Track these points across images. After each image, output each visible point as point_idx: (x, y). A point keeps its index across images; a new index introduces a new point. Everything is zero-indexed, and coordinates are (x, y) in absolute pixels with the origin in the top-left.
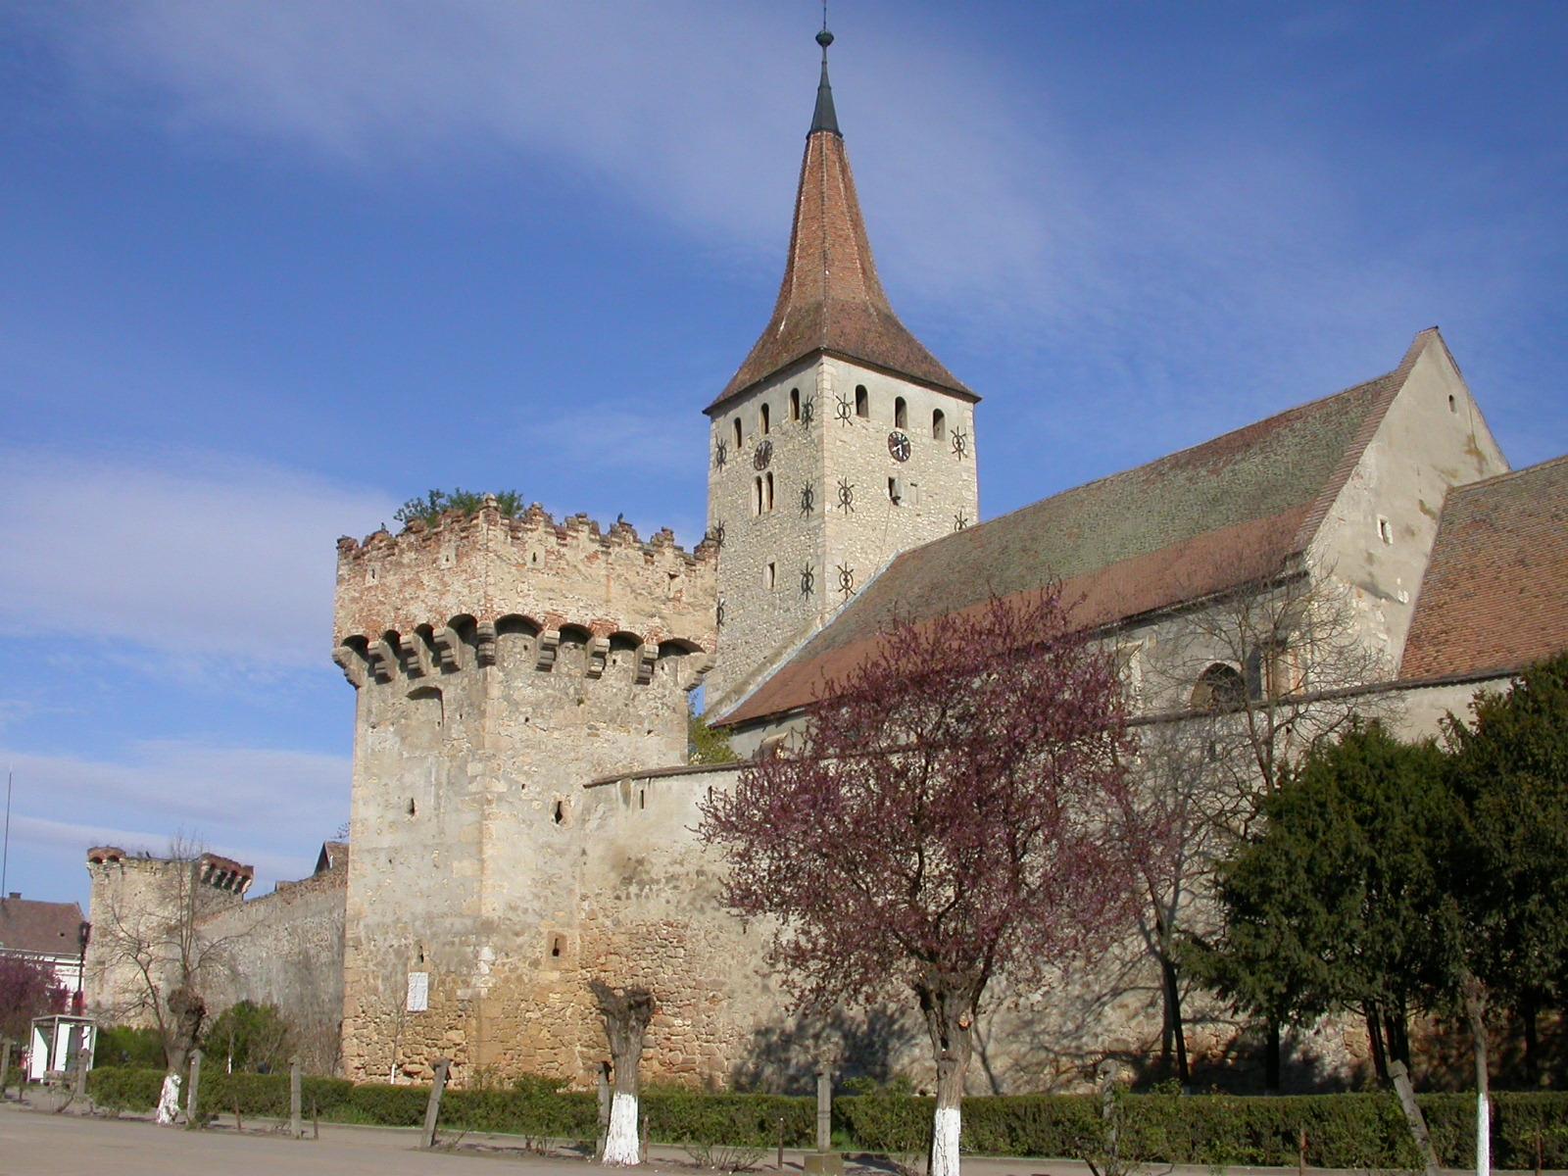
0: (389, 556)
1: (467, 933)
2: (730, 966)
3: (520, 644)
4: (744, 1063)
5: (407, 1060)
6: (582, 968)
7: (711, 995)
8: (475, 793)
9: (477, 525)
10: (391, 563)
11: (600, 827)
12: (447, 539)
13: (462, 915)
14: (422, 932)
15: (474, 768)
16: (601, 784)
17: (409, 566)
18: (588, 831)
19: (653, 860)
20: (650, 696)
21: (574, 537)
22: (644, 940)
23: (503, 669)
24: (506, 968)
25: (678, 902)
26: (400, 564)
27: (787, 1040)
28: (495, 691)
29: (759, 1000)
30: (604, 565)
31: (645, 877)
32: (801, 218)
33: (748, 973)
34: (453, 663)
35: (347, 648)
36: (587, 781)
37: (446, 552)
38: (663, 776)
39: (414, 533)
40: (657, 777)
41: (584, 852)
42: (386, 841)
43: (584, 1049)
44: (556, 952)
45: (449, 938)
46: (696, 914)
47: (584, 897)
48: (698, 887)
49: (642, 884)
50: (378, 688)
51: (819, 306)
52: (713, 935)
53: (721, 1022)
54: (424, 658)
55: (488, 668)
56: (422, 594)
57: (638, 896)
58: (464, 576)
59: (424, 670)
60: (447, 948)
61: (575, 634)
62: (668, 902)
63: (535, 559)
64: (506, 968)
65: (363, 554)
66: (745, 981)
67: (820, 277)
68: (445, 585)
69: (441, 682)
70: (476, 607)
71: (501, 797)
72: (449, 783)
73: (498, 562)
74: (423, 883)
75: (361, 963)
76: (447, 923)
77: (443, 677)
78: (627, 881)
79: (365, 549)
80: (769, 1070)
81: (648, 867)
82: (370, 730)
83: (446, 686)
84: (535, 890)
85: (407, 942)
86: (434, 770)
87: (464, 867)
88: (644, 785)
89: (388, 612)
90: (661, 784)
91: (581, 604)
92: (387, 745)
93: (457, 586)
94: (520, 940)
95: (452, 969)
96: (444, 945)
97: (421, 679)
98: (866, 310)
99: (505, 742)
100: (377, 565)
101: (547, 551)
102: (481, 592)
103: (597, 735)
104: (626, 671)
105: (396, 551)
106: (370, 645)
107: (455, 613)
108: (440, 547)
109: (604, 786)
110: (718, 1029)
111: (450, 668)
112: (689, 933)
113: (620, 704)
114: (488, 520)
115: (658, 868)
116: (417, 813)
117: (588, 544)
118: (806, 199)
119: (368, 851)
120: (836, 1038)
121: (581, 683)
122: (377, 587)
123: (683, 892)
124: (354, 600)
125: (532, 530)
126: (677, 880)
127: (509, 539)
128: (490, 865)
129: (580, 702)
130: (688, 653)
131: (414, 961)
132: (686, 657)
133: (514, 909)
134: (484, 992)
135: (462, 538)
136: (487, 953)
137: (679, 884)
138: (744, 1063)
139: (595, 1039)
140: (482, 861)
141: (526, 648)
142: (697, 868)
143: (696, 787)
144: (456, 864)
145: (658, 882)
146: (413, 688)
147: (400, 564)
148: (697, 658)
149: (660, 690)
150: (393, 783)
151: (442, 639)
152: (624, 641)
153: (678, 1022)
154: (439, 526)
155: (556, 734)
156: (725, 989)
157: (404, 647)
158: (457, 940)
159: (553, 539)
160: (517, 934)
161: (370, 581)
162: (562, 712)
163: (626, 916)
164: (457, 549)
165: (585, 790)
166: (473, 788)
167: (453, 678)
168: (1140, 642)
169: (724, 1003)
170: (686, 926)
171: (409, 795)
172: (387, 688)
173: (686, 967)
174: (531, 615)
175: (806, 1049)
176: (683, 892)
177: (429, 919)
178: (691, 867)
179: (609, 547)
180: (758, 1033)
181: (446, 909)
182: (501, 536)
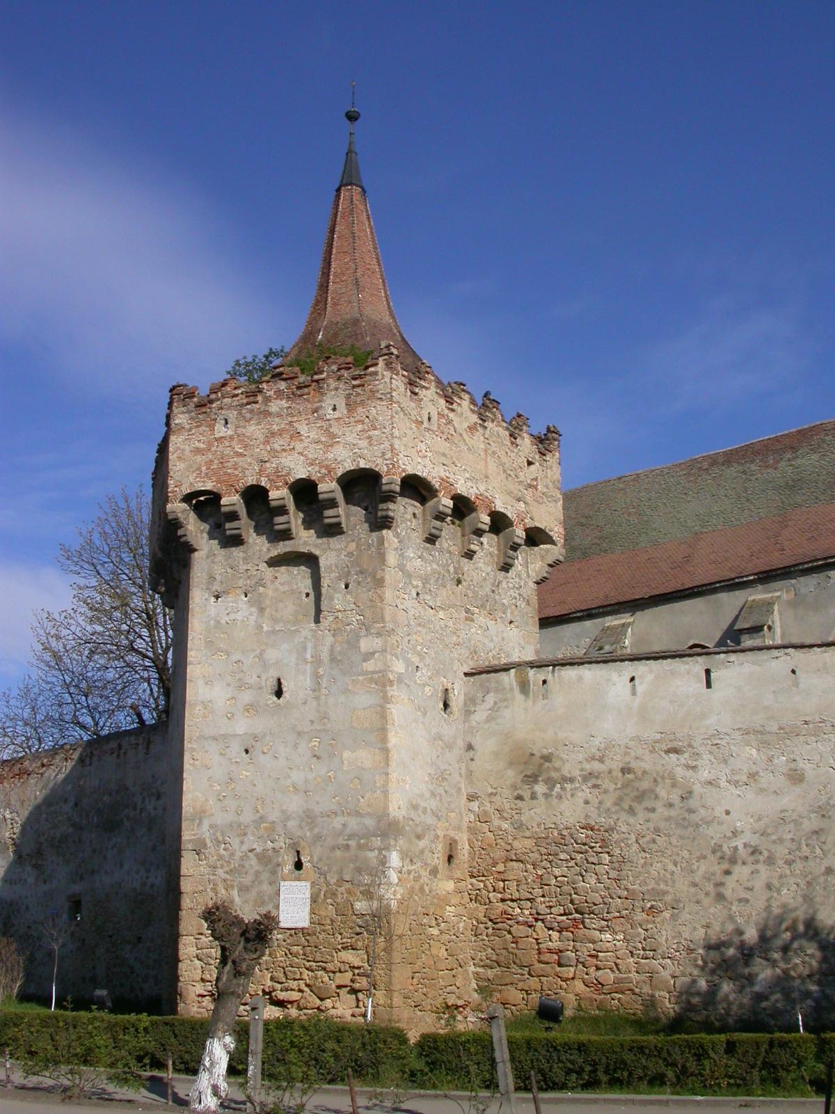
0: (248, 404)
1: (368, 835)
2: (672, 873)
3: (410, 510)
4: (694, 982)
5: (278, 986)
6: (472, 876)
7: (649, 905)
8: (373, 672)
9: (376, 373)
10: (251, 411)
11: (488, 720)
12: (332, 387)
13: (358, 814)
14: (299, 833)
15: (366, 644)
16: (488, 672)
17: (279, 415)
18: (474, 723)
19: (564, 756)
20: (511, 585)
21: (459, 404)
22: (554, 844)
23: (397, 535)
24: (411, 877)
25: (600, 803)
26: (267, 414)
27: (747, 954)
28: (392, 559)
29: (712, 910)
30: (482, 438)
31: (554, 775)
32: (334, 251)
33: (697, 880)
34: (339, 524)
35: (185, 505)
36: (466, 671)
37: (333, 399)
38: (572, 664)
39: (285, 380)
40: (563, 665)
41: (470, 747)
42: (241, 726)
43: (481, 970)
44: (450, 858)
45: (341, 841)
46: (624, 816)
47: (471, 798)
48: (624, 786)
49: (551, 783)
50: (223, 552)
51: (356, 322)
52: (647, 838)
53: (665, 935)
54: (295, 519)
55: (384, 532)
56: (299, 447)
57: (547, 796)
58: (360, 427)
59: (294, 531)
60: (338, 853)
61: (463, 507)
62: (587, 802)
63: (429, 419)
64: (411, 877)
65: (211, 402)
66: (692, 890)
67: (354, 298)
68: (333, 436)
69: (316, 546)
70: (379, 461)
71: (400, 679)
72: (333, 659)
73: (401, 414)
74: (297, 777)
75: (204, 870)
76: (337, 822)
77: (320, 541)
78: (532, 779)
79: (213, 396)
80: (726, 987)
81: (557, 764)
82: (213, 599)
83: (324, 551)
84: (431, 787)
85: (276, 845)
86: (310, 645)
87: (365, 757)
88: (546, 673)
89: (250, 464)
90: (570, 673)
91: (467, 475)
92: (239, 616)
93: (351, 437)
94: (422, 844)
95: (347, 877)
96: (333, 849)
97: (291, 542)
98: (391, 330)
99: (401, 617)
100: (232, 415)
101: (439, 414)
102: (387, 444)
103: (472, 620)
104: (491, 554)
105: (260, 398)
106: (224, 501)
107: (349, 466)
108: (323, 394)
109: (493, 674)
110: (661, 944)
111: (333, 530)
112: (615, 836)
113: (488, 590)
114: (389, 365)
115: (571, 764)
116: (286, 695)
117: (469, 413)
118: (339, 237)
119: (215, 739)
120: (812, 949)
121: (458, 562)
122: (231, 438)
123: (606, 792)
124: (198, 451)
125: (427, 388)
126: (597, 778)
127: (409, 393)
128: (394, 756)
129: (459, 582)
130: (537, 545)
131: (289, 867)
132: (536, 548)
133: (415, 807)
134: (394, 904)
135: (354, 387)
136: (395, 859)
137: (599, 782)
138: (694, 982)
139: (494, 958)
140: (386, 751)
141: (414, 515)
142: (621, 765)
143: (614, 676)
144: (346, 754)
145: (571, 780)
146: (274, 553)
147: (267, 414)
148: (548, 550)
149: (517, 580)
150: (249, 660)
151: (331, 495)
152: (499, 523)
153: (607, 936)
154: (321, 372)
155: (441, 614)
156: (668, 898)
157: (273, 504)
158: (352, 843)
159: (442, 402)
160: (419, 837)
161: (220, 430)
162: (444, 589)
163: (532, 819)
164: (348, 397)
165: (465, 679)
166: (370, 666)
167: (335, 542)
168: (778, 594)
169: (667, 914)
170: (610, 830)
171: (274, 674)
172: (236, 552)
173: (613, 874)
174: (429, 479)
175: (774, 963)
176: (606, 792)
177: (309, 818)
178: (615, 763)
179: (484, 421)
180: (709, 947)
181: (334, 807)
182: (402, 388)
